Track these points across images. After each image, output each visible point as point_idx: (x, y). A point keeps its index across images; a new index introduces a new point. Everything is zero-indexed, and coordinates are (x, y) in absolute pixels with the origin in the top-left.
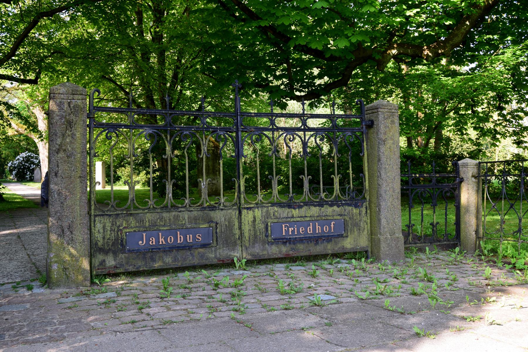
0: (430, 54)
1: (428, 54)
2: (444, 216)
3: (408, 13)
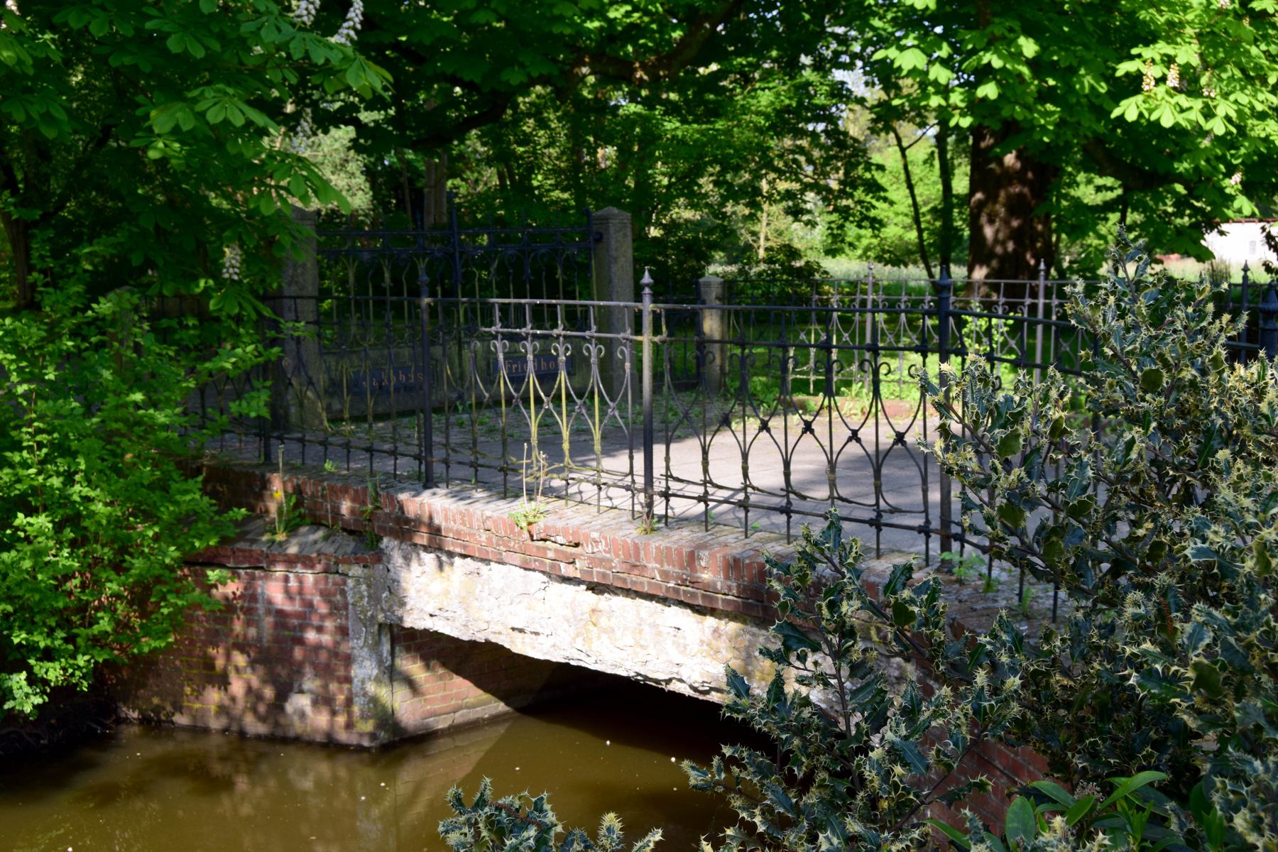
0: (645, 77)
1: (641, 78)
2: (919, 199)
3: (612, 14)
